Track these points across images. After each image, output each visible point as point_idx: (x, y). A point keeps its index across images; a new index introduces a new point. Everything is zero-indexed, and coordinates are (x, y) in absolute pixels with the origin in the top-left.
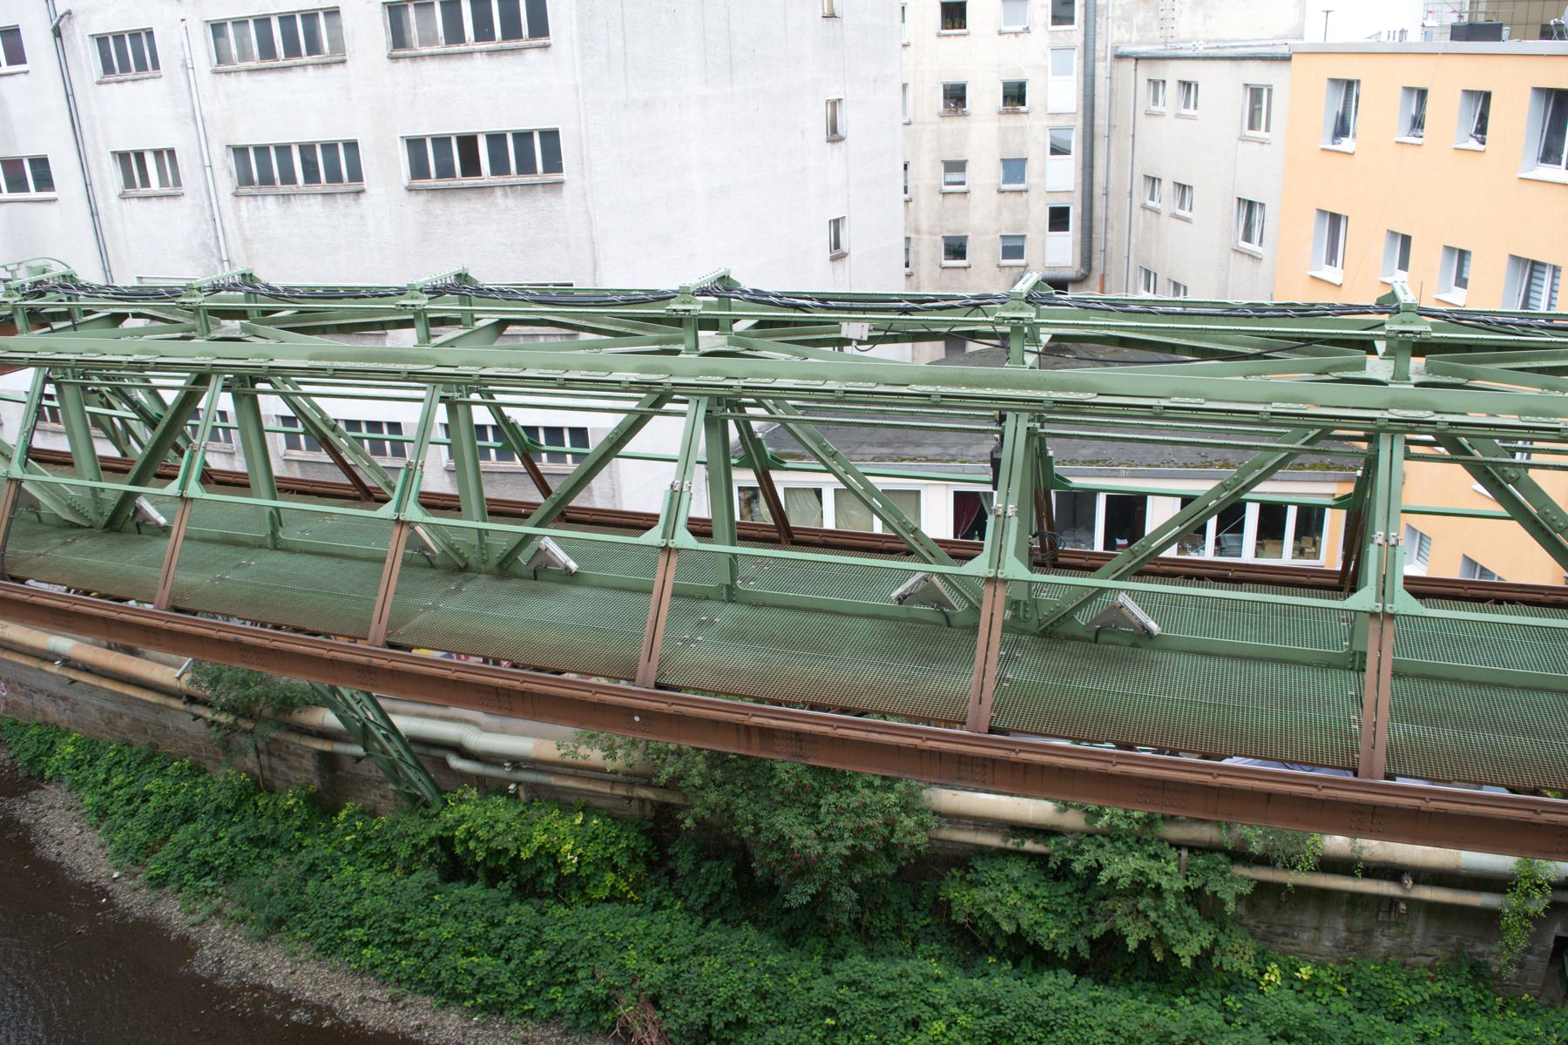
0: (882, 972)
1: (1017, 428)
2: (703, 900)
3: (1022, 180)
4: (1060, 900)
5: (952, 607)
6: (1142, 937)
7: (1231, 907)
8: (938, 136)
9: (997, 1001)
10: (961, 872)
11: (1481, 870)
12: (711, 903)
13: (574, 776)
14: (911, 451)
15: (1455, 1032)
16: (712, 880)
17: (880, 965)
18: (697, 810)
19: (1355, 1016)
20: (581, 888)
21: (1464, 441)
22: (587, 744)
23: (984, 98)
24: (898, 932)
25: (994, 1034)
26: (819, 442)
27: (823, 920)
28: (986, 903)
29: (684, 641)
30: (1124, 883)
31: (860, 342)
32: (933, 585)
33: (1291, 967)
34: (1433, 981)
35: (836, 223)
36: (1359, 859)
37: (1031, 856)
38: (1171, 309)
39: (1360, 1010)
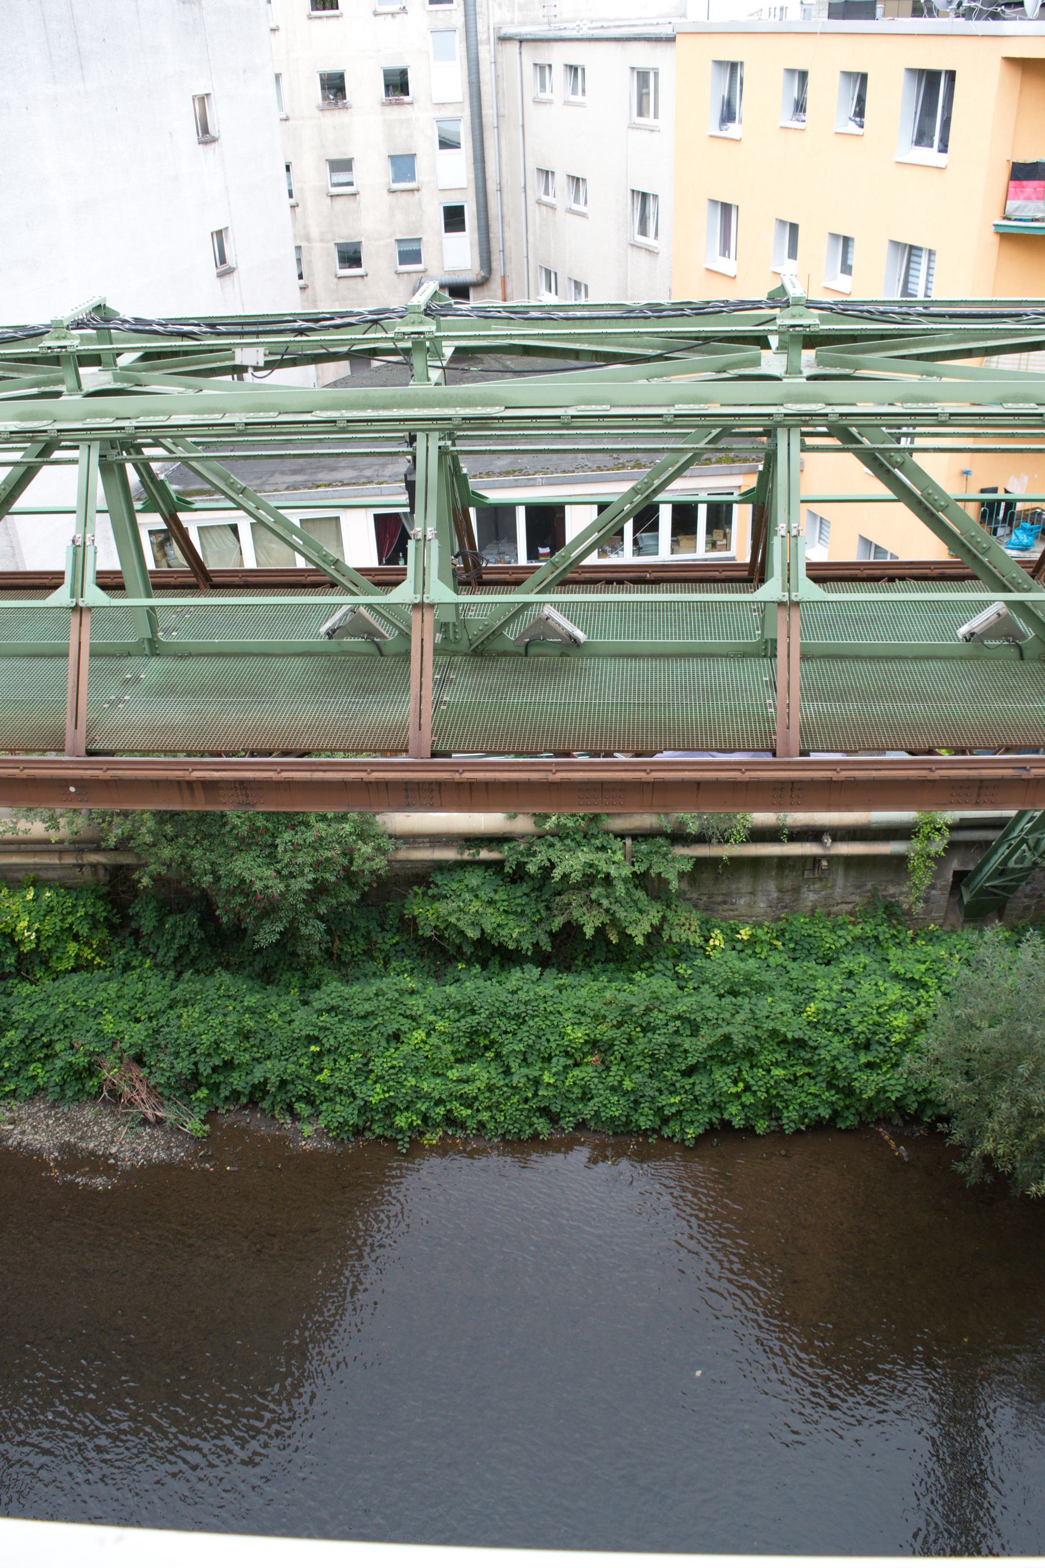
0: (358, 995)
1: (429, 447)
2: (172, 954)
3: (412, 178)
4: (519, 901)
5: (384, 637)
6: (598, 924)
7: (674, 885)
8: (321, 131)
9: (470, 1003)
10: (423, 889)
11: (889, 822)
12: (181, 956)
13: (18, 852)
14: (324, 476)
15: (876, 966)
16: (178, 934)
17: (356, 988)
18: (152, 867)
19: (791, 965)
20: (45, 963)
21: (854, 430)
22: (27, 817)
23: (365, 87)
24: (368, 953)
25: (471, 1034)
26: (225, 479)
27: (294, 954)
28: (450, 914)
29: (111, 703)
30: (576, 877)
31: (256, 369)
32: (361, 615)
33: (732, 930)
34: (854, 924)
35: (219, 235)
36: (784, 826)
37: (487, 864)
38: (571, 314)
39: (794, 959)
